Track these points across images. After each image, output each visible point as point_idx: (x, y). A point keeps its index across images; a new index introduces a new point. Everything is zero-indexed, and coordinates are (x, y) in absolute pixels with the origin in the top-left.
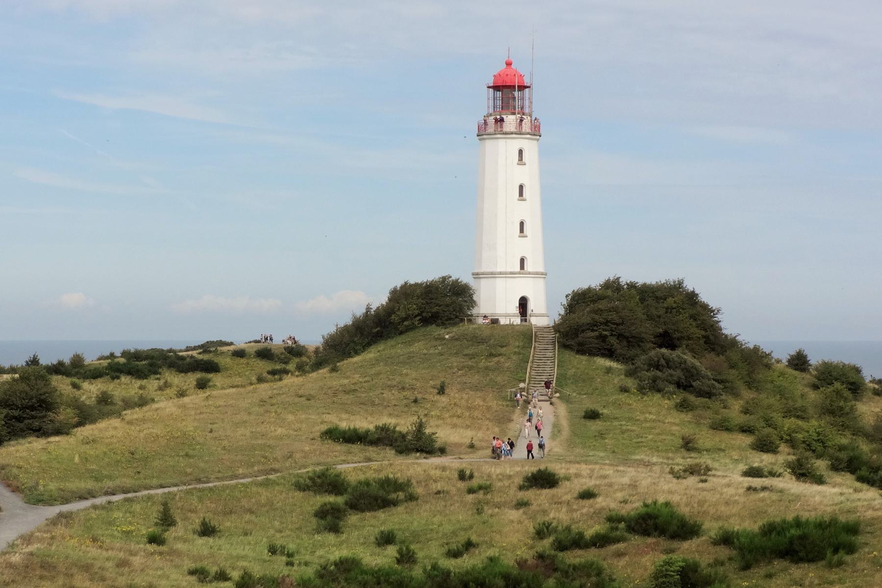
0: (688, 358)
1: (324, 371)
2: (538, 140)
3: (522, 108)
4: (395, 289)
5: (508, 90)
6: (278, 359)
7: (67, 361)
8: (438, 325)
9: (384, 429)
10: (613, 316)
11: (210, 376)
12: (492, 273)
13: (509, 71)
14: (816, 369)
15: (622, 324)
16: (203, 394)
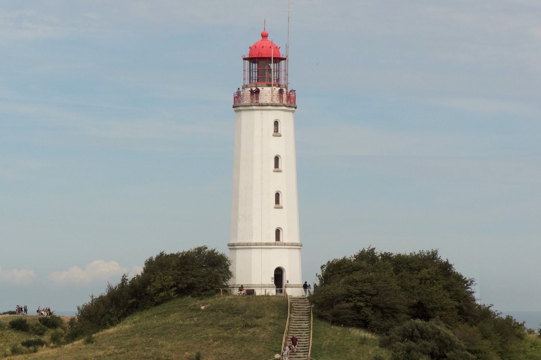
0: (442, 328)
3: (278, 80)
5: (263, 63)
10: (367, 287)
12: (247, 244)
13: (264, 44)
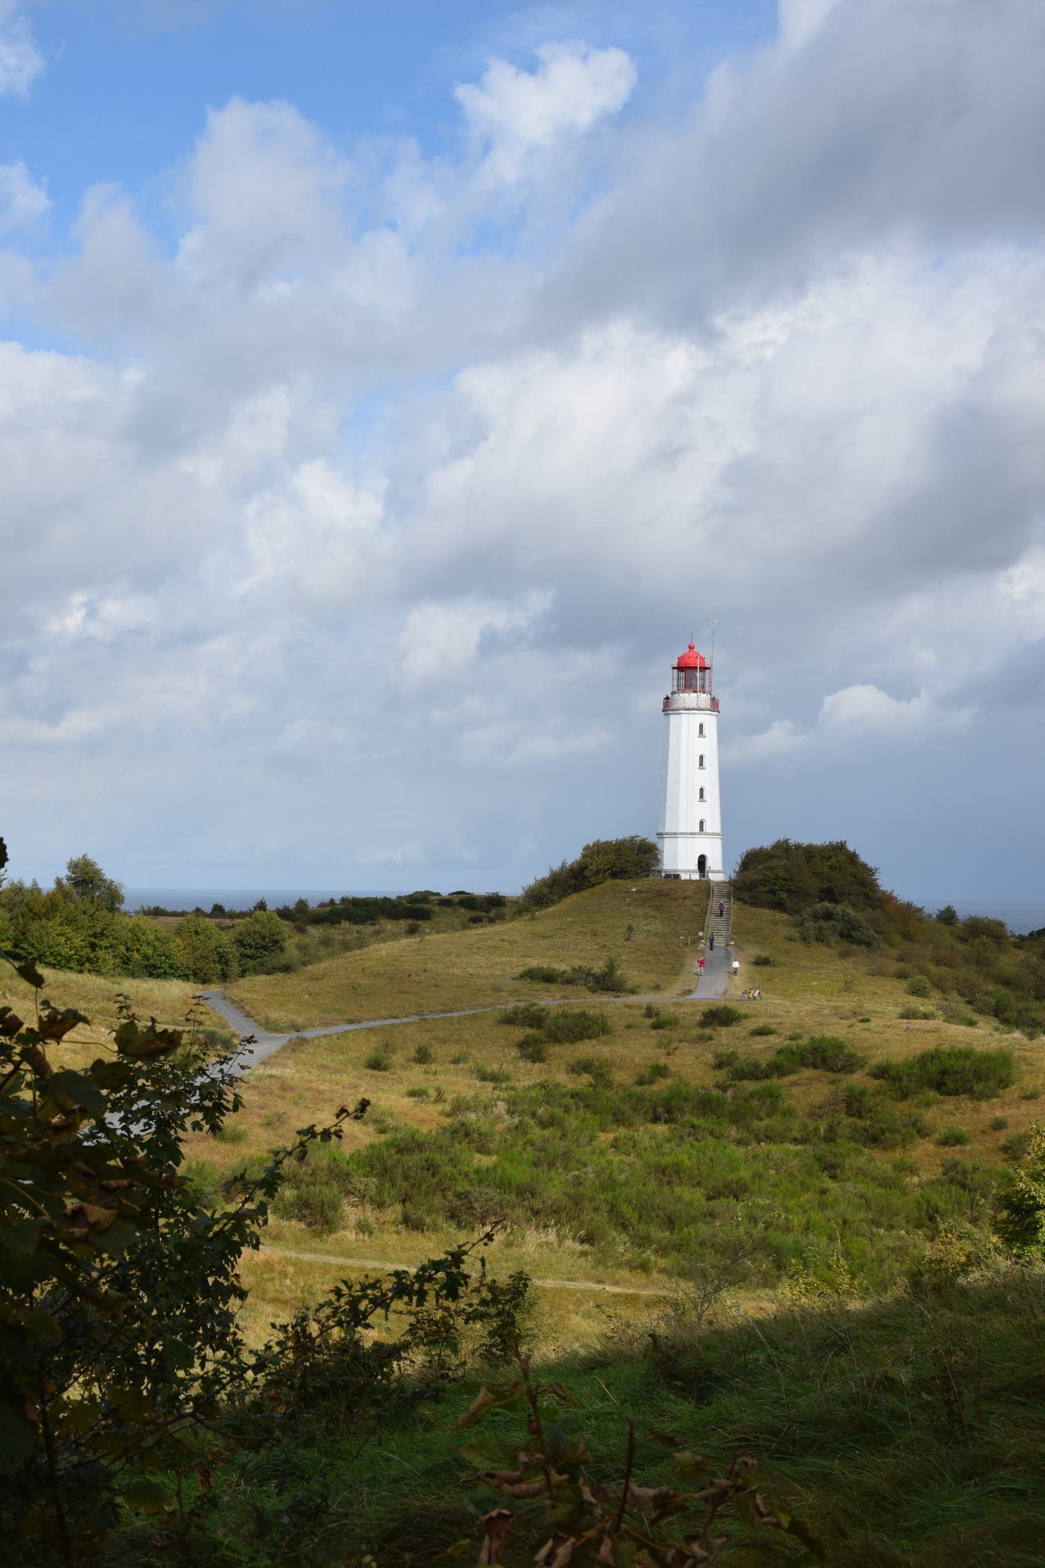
0: (851, 911)
3: (703, 687)
6: (481, 909)
7: (292, 906)
11: (420, 922)
12: (674, 834)
14: (964, 925)
15: (790, 880)
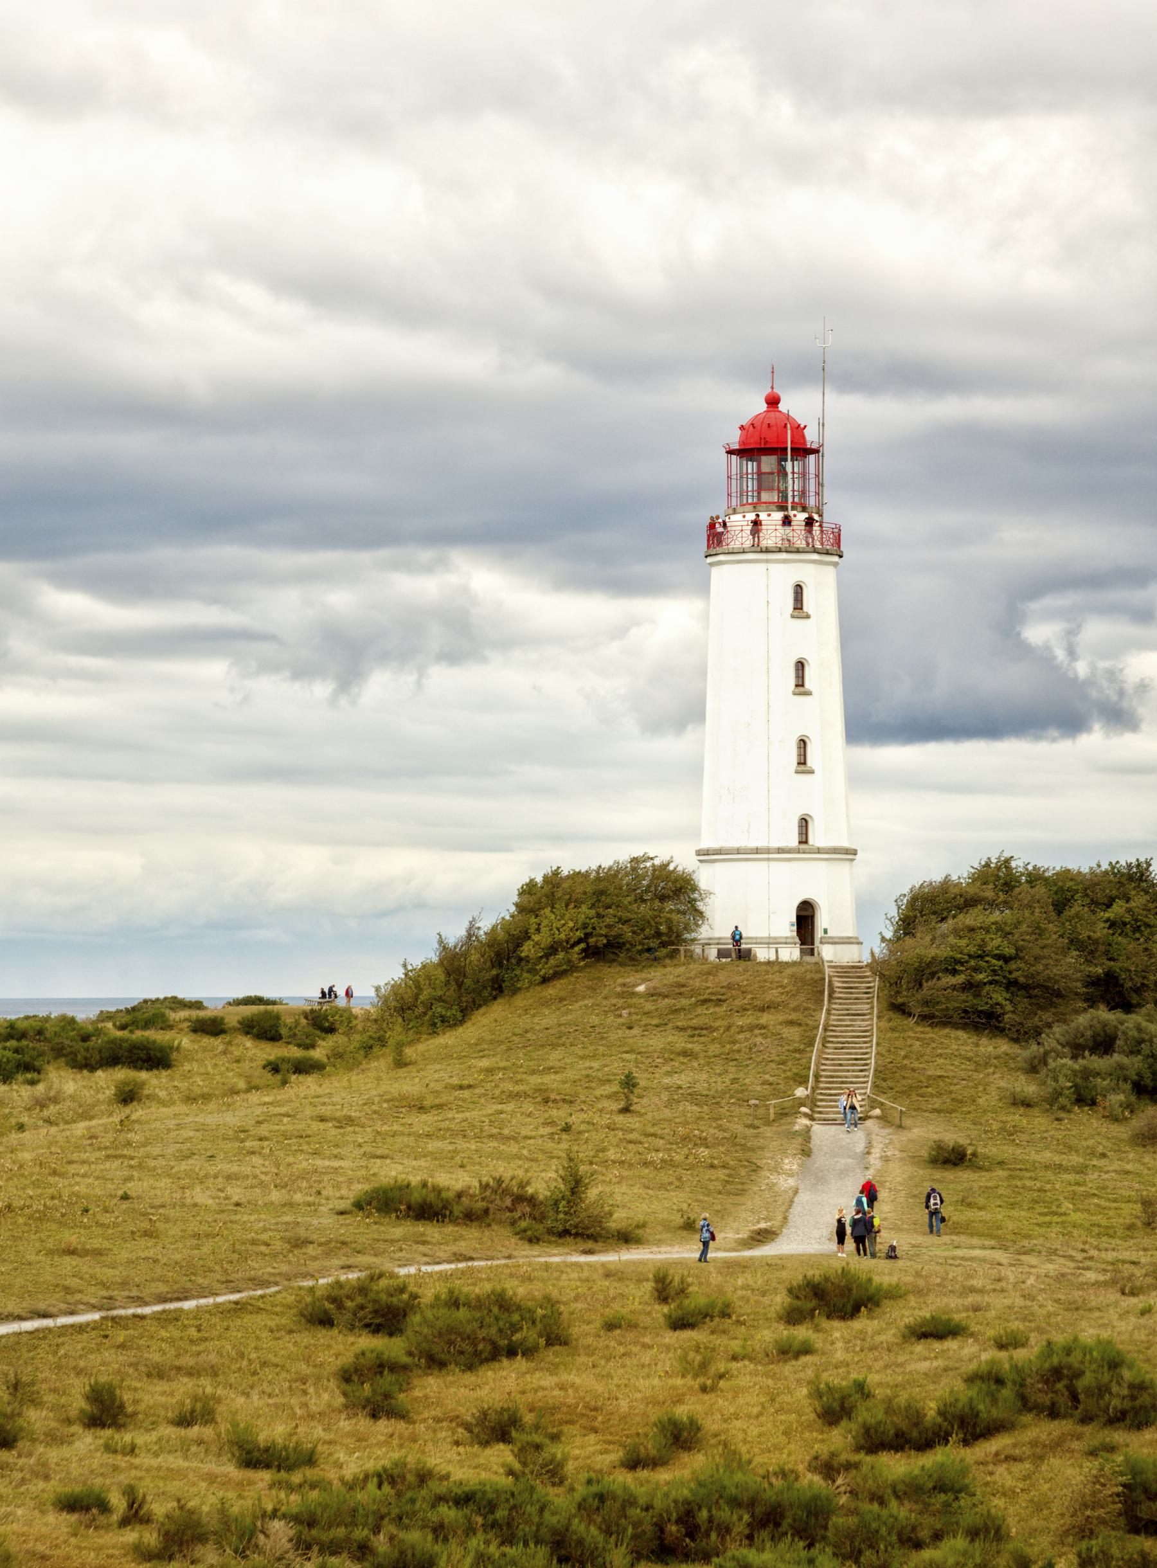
1: (380, 1064)
2: (835, 564)
3: (803, 493)
4: (531, 885)
6: (291, 1039)
8: (622, 965)
9: (498, 1187)
10: (995, 942)
16: (121, 1113)
